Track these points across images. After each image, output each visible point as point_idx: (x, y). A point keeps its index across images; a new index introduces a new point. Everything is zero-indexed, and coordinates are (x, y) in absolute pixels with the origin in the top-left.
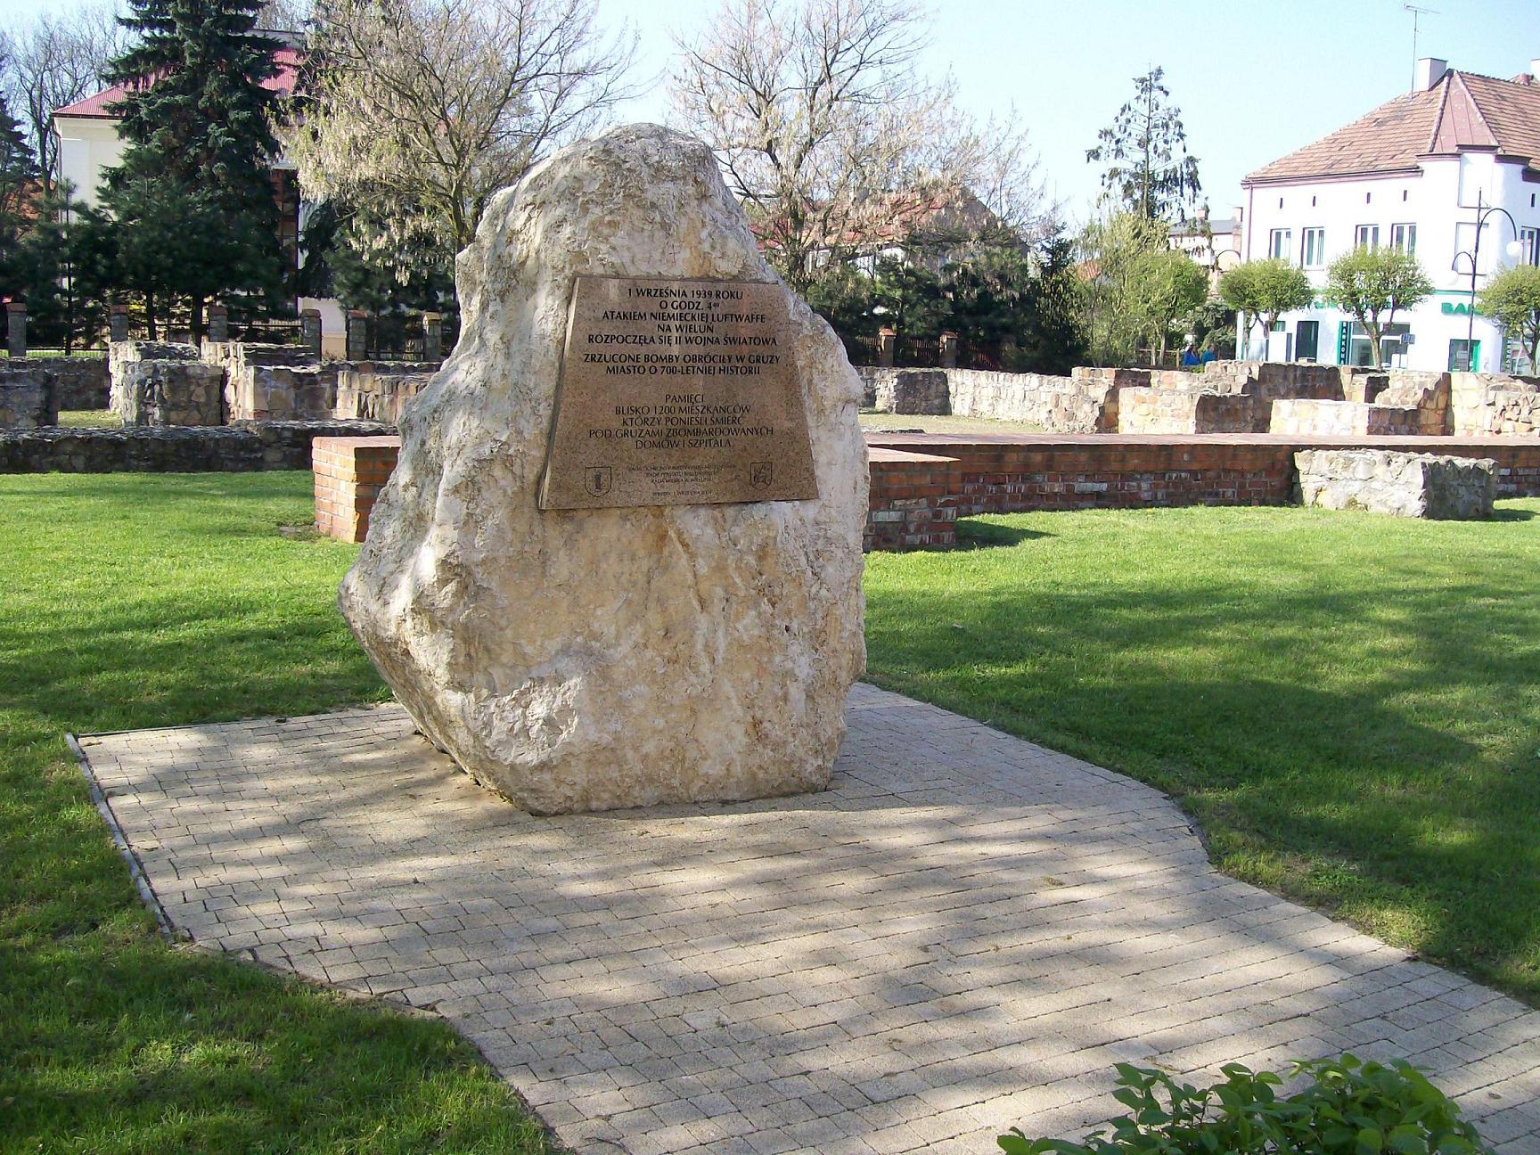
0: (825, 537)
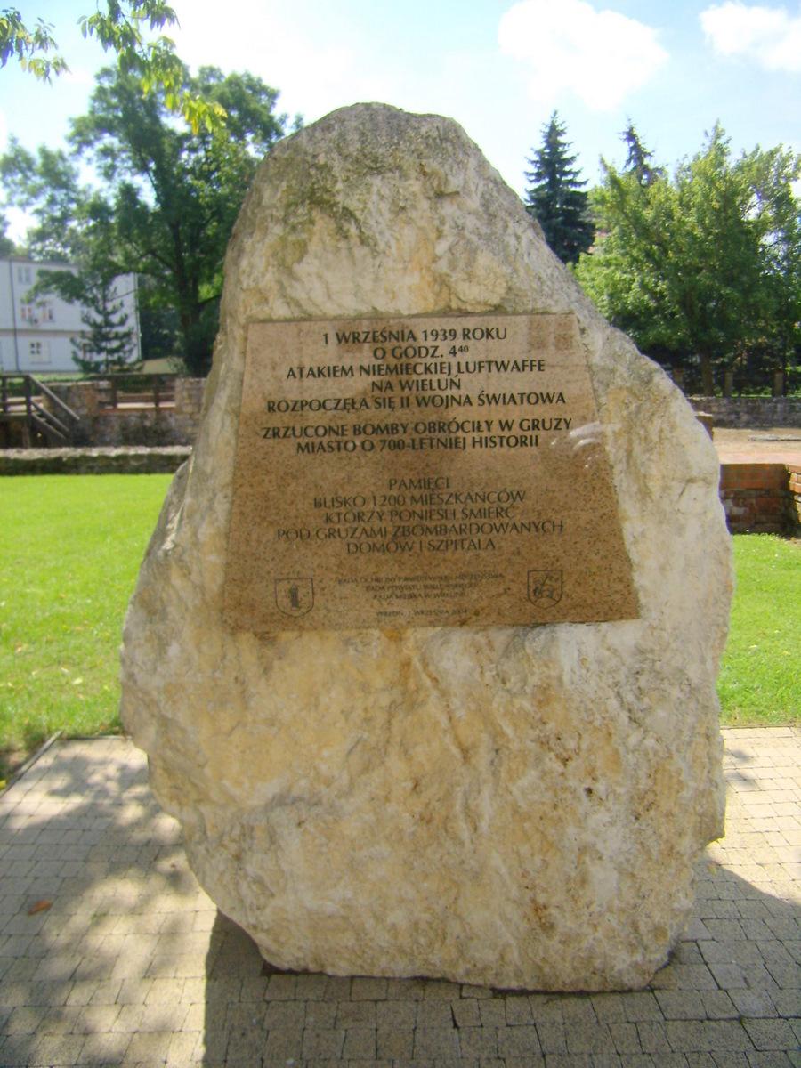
0: (652, 670)
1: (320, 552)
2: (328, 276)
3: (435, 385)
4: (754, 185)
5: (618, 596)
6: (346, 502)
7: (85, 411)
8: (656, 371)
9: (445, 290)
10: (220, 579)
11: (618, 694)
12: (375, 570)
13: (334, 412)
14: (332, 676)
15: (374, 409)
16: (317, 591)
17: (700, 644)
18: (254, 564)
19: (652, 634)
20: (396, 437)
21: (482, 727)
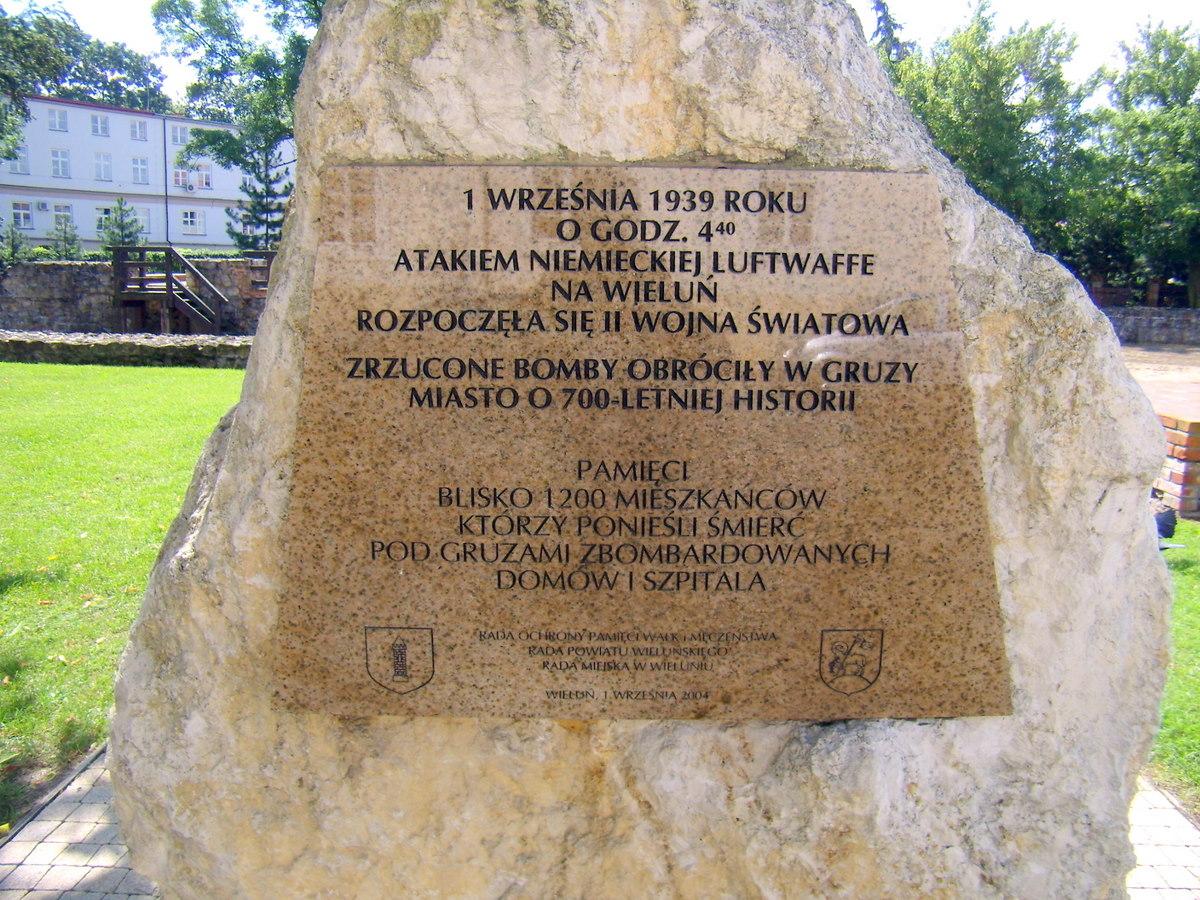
0: (1026, 798)
1: (446, 584)
2: (477, 82)
3: (670, 292)
4: (1022, 65)
5: (977, 677)
6: (496, 498)
7: (235, 292)
8: (1068, 283)
9: (696, 118)
10: (272, 619)
11: (966, 839)
12: (546, 619)
13: (480, 334)
14: (466, 785)
15: (553, 332)
16: (441, 651)
17: (1111, 757)
18: (329, 598)
19: (1030, 737)
20: (592, 385)
21: (724, 882)
